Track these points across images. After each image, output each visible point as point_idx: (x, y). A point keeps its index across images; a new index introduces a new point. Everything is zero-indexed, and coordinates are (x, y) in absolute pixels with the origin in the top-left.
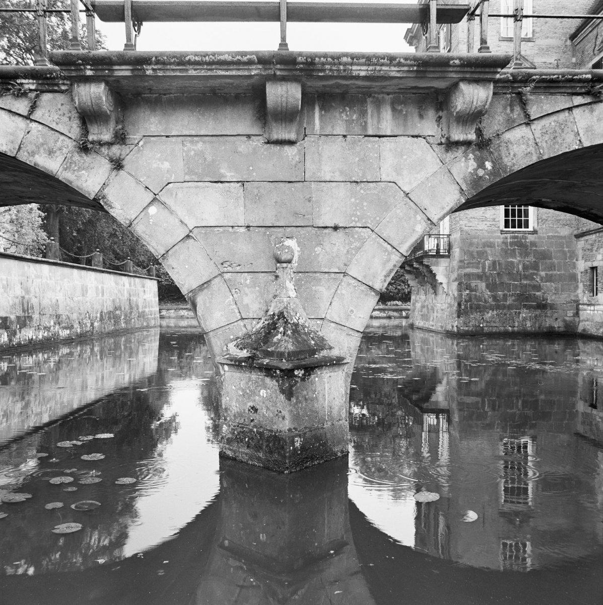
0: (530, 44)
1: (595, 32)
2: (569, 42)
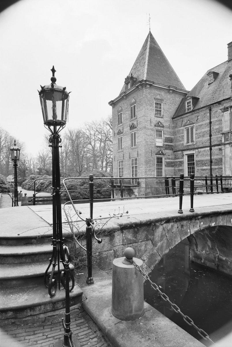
0: (162, 119)
1: (182, 119)
2: (172, 120)
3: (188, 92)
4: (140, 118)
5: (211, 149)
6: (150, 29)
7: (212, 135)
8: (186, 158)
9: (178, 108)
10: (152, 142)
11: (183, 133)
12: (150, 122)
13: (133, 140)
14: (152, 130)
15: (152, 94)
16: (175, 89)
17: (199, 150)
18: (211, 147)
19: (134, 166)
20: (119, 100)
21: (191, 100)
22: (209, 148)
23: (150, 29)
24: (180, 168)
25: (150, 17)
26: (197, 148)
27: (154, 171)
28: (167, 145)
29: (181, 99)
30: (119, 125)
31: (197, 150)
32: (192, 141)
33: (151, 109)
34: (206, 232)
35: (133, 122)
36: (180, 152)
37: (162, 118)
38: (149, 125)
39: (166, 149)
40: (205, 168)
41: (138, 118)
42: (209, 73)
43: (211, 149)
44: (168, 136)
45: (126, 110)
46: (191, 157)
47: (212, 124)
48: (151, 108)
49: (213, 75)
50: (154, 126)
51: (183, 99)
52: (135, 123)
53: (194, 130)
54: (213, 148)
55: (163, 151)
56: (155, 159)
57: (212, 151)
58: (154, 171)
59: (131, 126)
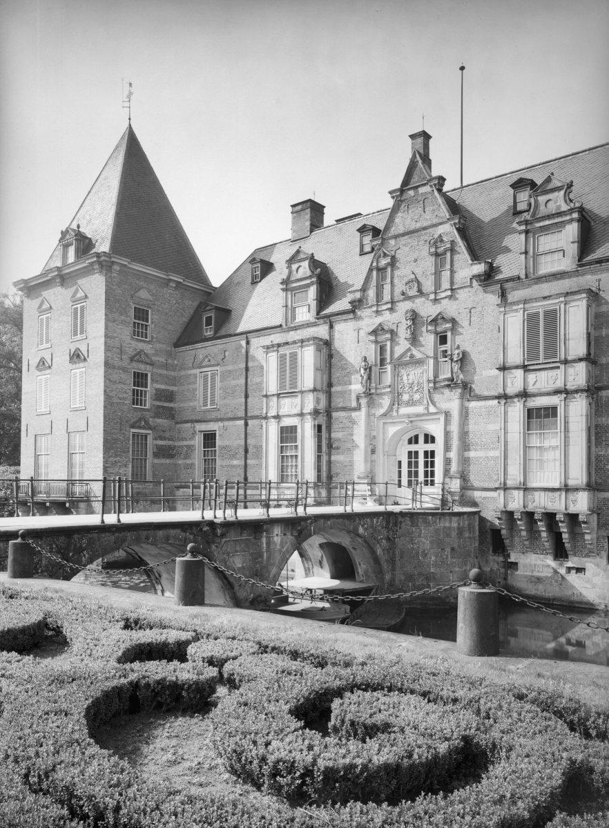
1: (194, 352)
3: (214, 290)
4: (94, 338)
5: (246, 424)
6: (130, 119)
7: (250, 394)
8: (198, 441)
9: (188, 323)
10: (124, 399)
11: (195, 383)
12: (118, 351)
13: (79, 320)
14: (125, 370)
15: (126, 287)
16: (182, 281)
17: (226, 423)
18: (246, 419)
19: (413, 469)
20: (43, 282)
21: (212, 314)
22: (242, 422)
23: (130, 119)
24: (189, 462)
25: (132, 91)
26: (222, 420)
27: (126, 466)
28: (159, 407)
29: (196, 304)
30: (41, 347)
31: (221, 424)
32: (213, 403)
33: (123, 322)
34: (11, 388)
35: (78, 345)
36: (189, 425)
37: (149, 342)
38: (116, 359)
39: (157, 415)
40: (235, 462)
41: (89, 337)
42: (252, 260)
43: (246, 424)
44: (163, 387)
45: (61, 313)
46: (210, 439)
47: (250, 373)
48: (123, 318)
49: (311, 211)
50: (128, 361)
51: (201, 303)
52: (84, 349)
53: (218, 379)
54: (250, 422)
55: (151, 419)
56: (129, 437)
57: (248, 428)
58: (126, 466)
59: (72, 353)
